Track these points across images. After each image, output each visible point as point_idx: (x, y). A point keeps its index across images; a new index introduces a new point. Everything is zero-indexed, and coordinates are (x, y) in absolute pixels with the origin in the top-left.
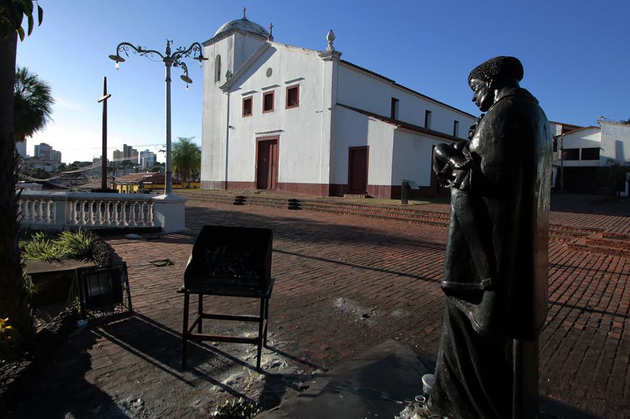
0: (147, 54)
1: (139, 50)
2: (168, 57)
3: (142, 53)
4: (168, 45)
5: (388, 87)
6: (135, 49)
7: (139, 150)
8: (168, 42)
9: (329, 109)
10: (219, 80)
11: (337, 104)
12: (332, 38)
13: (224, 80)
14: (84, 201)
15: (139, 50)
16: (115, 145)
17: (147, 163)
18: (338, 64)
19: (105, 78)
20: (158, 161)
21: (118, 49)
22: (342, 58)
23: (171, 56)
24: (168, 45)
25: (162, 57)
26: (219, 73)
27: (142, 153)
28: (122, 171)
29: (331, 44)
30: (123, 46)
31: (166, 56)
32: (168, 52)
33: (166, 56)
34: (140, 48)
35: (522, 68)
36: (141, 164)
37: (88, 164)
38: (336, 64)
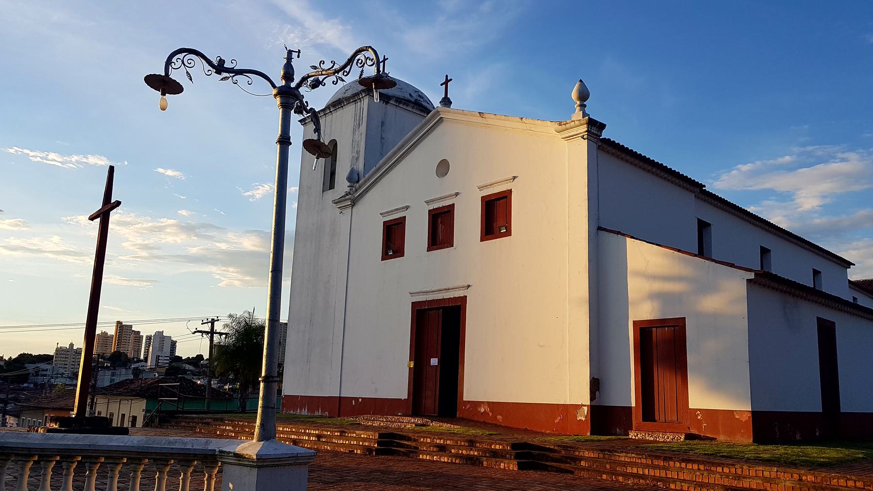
0: (238, 78)
1: (220, 68)
2: (287, 86)
3: (225, 75)
4: (289, 58)
5: (689, 198)
6: (209, 63)
7: (144, 334)
8: (290, 53)
9: (72, 345)
10: (332, 186)
11: (600, 228)
12: (583, 96)
13: (342, 185)
14: (32, 456)
15: (220, 68)
16: (106, 326)
17: (158, 357)
18: (599, 148)
19: (112, 169)
20: (178, 353)
21: (169, 62)
22: (605, 135)
23: (293, 85)
24: (289, 58)
25: (274, 86)
26: (333, 174)
27: (149, 338)
28: (110, 373)
29: (583, 106)
30: (181, 56)
31: (283, 83)
32: (288, 74)
33: (283, 83)
34: (222, 62)
35: (24, 354)
36: (146, 359)
37: (46, 359)
38: (595, 146)
